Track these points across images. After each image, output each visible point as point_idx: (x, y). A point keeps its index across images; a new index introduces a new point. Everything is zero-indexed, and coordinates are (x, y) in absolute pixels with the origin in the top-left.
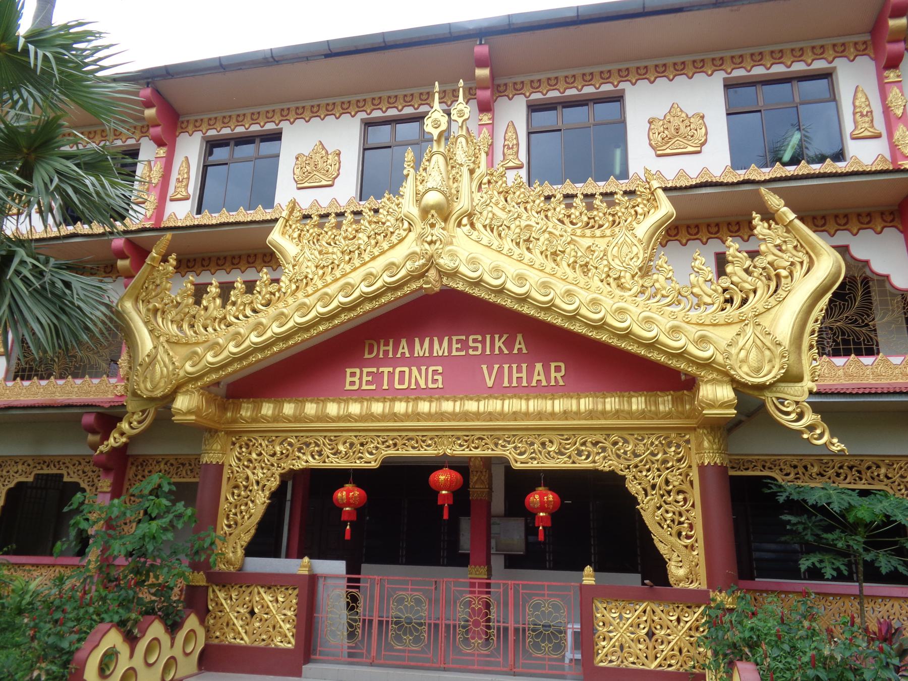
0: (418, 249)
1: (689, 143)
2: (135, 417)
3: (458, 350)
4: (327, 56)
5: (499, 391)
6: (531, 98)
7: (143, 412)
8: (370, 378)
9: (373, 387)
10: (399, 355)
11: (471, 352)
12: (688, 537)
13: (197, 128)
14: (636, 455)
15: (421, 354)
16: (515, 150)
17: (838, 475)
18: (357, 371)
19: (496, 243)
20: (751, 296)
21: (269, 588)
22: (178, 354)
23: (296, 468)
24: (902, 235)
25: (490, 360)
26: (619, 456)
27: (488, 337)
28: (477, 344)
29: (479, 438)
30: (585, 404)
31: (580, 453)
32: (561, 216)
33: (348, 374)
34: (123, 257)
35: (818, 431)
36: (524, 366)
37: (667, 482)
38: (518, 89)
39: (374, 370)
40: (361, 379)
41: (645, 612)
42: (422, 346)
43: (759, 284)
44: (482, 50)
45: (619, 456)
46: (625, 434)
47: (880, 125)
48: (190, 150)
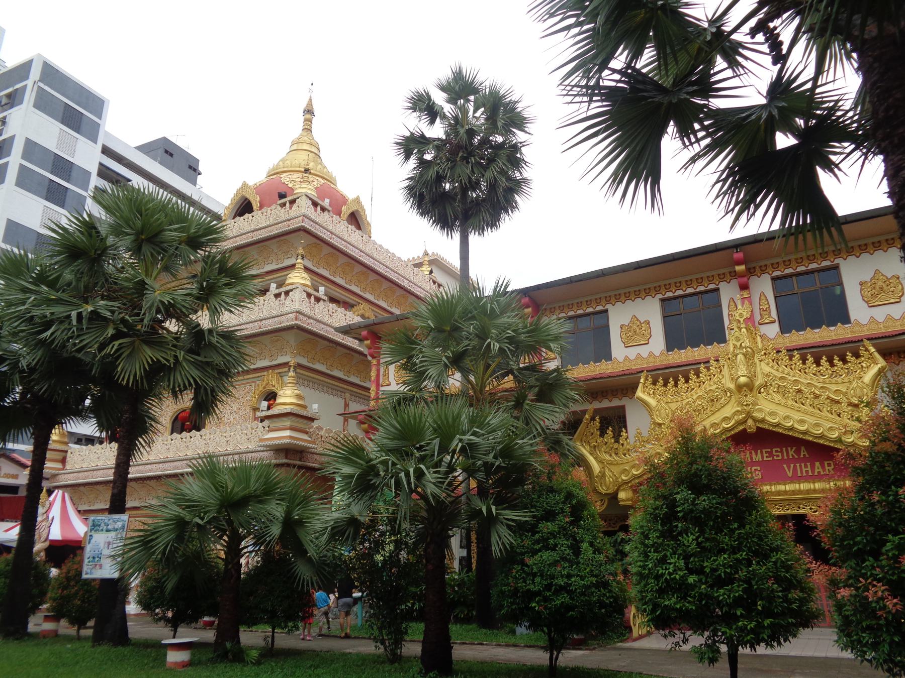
0: (739, 409)
5: (795, 479)
19: (783, 401)
22: (616, 470)
25: (788, 461)
28: (778, 454)
36: (808, 464)
38: (764, 270)
44: (739, 255)
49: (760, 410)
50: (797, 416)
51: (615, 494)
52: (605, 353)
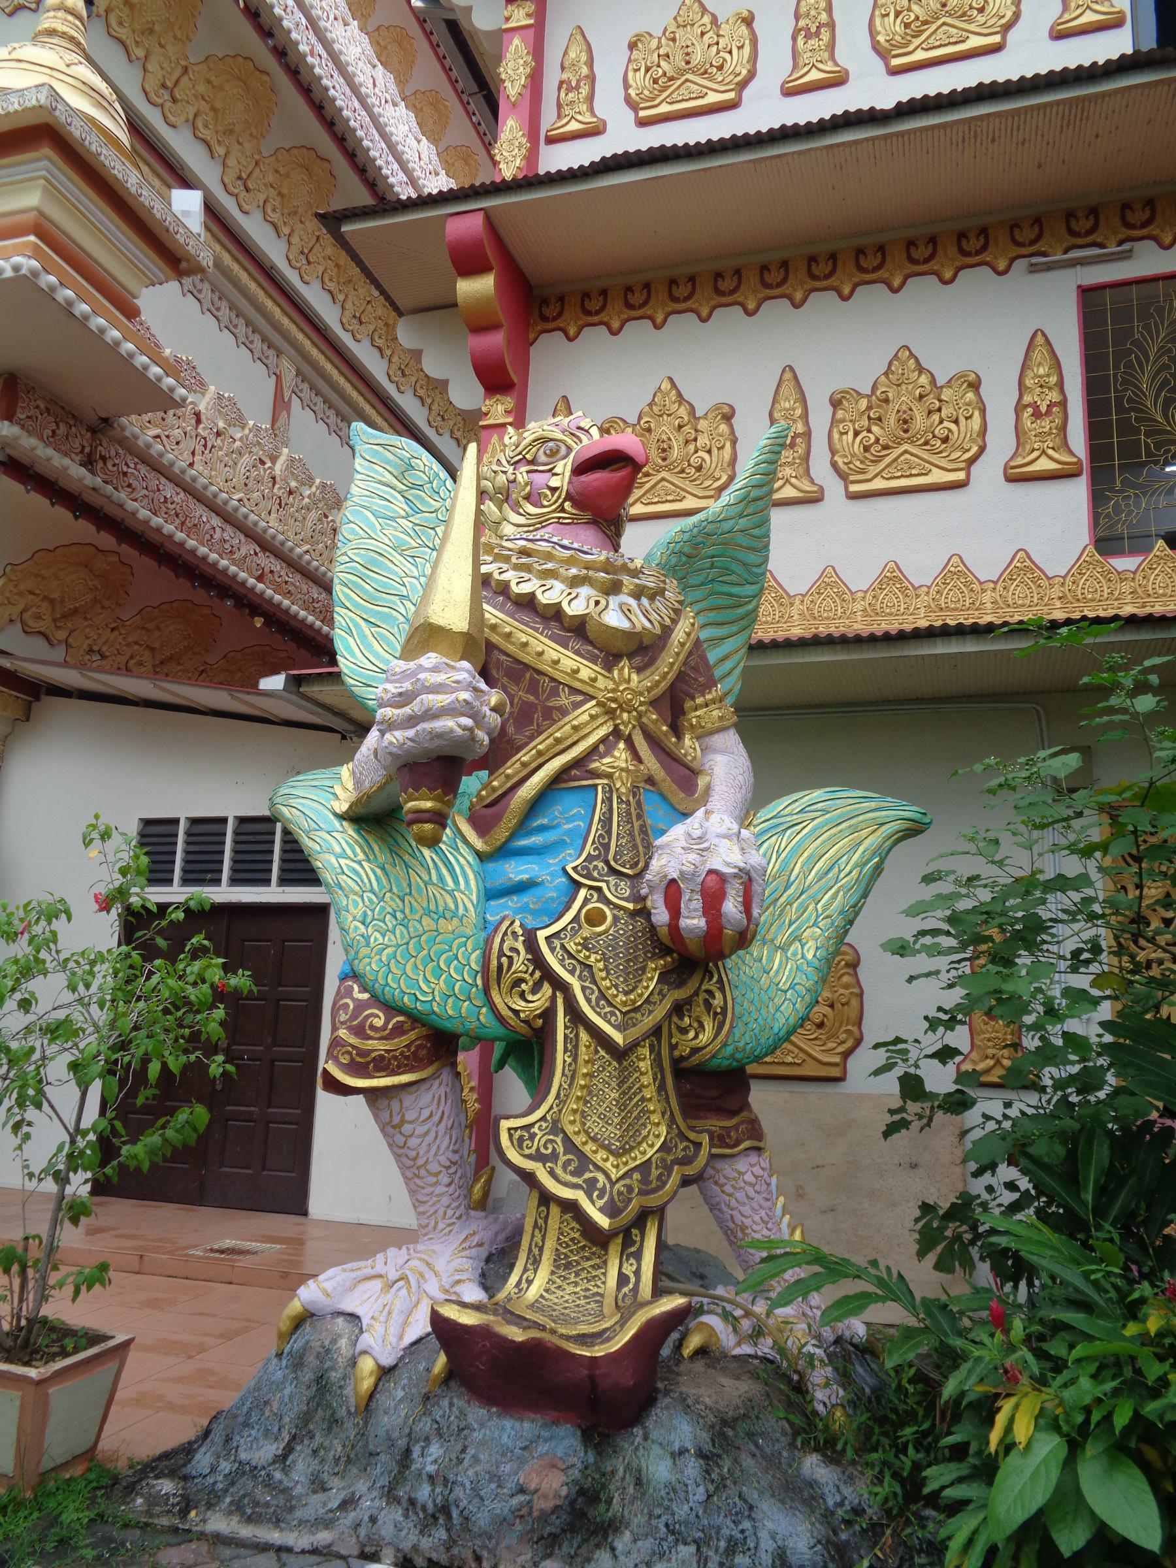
1: (934, 459)
16: (800, 450)
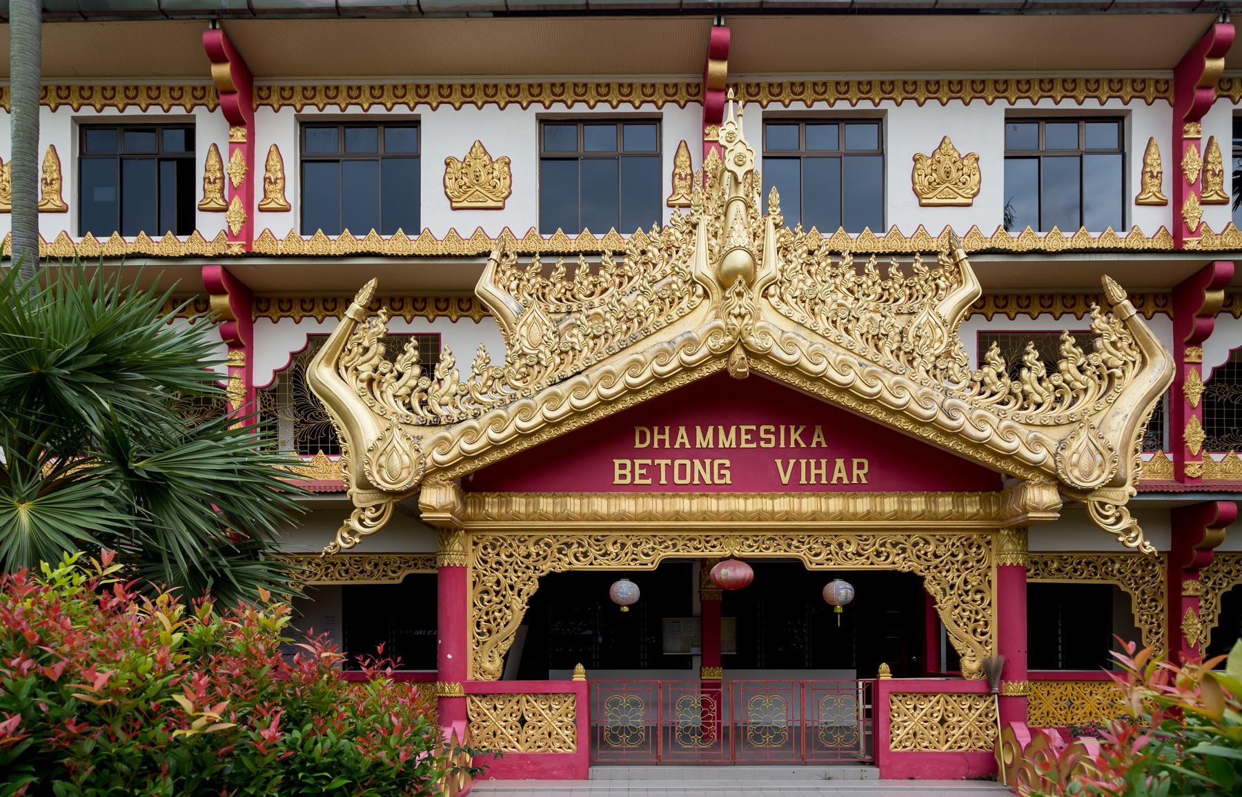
2: (368, 513)
3: (747, 441)
4: (497, 14)
5: (795, 488)
6: (768, 109)
7: (377, 507)
8: (644, 471)
9: (649, 481)
10: (677, 446)
11: (762, 444)
12: (983, 634)
13: (285, 100)
14: (936, 556)
15: (704, 445)
17: (1075, 570)
18: (628, 462)
20: (1082, 397)
21: (484, 696)
23: (558, 571)
24: (1171, 323)
25: (785, 454)
26: (919, 557)
27: (782, 428)
28: (769, 437)
29: (769, 539)
30: (890, 504)
31: (878, 554)
32: (850, 285)
33: (617, 466)
34: (220, 292)
35: (1133, 535)
36: (824, 462)
37: (966, 582)
39: (649, 462)
40: (633, 472)
41: (938, 702)
42: (704, 435)
43: (1091, 383)
45: (919, 557)
46: (926, 535)
47: (1167, 193)
48: (278, 132)
49: (765, 332)
50: (835, 354)
51: (414, 492)
52: (403, 212)
